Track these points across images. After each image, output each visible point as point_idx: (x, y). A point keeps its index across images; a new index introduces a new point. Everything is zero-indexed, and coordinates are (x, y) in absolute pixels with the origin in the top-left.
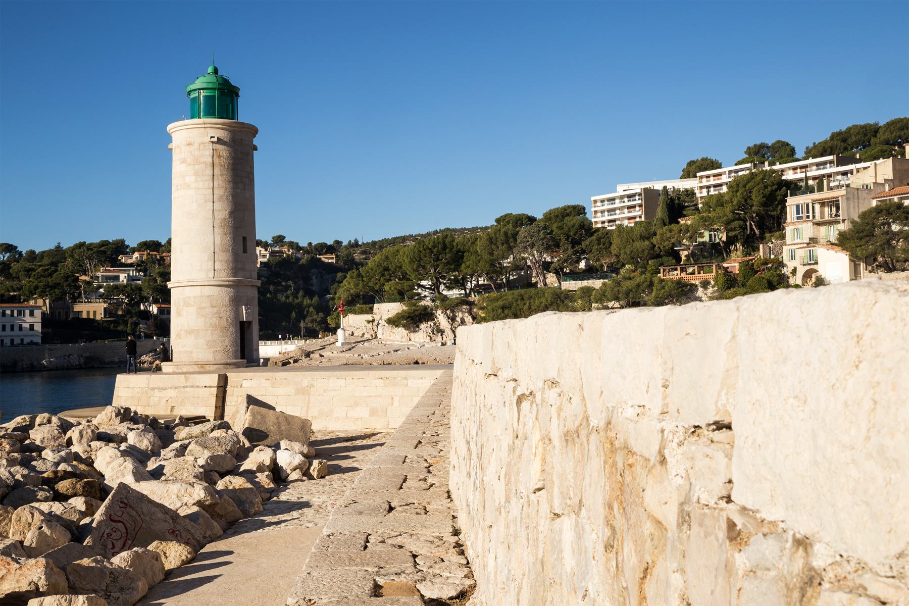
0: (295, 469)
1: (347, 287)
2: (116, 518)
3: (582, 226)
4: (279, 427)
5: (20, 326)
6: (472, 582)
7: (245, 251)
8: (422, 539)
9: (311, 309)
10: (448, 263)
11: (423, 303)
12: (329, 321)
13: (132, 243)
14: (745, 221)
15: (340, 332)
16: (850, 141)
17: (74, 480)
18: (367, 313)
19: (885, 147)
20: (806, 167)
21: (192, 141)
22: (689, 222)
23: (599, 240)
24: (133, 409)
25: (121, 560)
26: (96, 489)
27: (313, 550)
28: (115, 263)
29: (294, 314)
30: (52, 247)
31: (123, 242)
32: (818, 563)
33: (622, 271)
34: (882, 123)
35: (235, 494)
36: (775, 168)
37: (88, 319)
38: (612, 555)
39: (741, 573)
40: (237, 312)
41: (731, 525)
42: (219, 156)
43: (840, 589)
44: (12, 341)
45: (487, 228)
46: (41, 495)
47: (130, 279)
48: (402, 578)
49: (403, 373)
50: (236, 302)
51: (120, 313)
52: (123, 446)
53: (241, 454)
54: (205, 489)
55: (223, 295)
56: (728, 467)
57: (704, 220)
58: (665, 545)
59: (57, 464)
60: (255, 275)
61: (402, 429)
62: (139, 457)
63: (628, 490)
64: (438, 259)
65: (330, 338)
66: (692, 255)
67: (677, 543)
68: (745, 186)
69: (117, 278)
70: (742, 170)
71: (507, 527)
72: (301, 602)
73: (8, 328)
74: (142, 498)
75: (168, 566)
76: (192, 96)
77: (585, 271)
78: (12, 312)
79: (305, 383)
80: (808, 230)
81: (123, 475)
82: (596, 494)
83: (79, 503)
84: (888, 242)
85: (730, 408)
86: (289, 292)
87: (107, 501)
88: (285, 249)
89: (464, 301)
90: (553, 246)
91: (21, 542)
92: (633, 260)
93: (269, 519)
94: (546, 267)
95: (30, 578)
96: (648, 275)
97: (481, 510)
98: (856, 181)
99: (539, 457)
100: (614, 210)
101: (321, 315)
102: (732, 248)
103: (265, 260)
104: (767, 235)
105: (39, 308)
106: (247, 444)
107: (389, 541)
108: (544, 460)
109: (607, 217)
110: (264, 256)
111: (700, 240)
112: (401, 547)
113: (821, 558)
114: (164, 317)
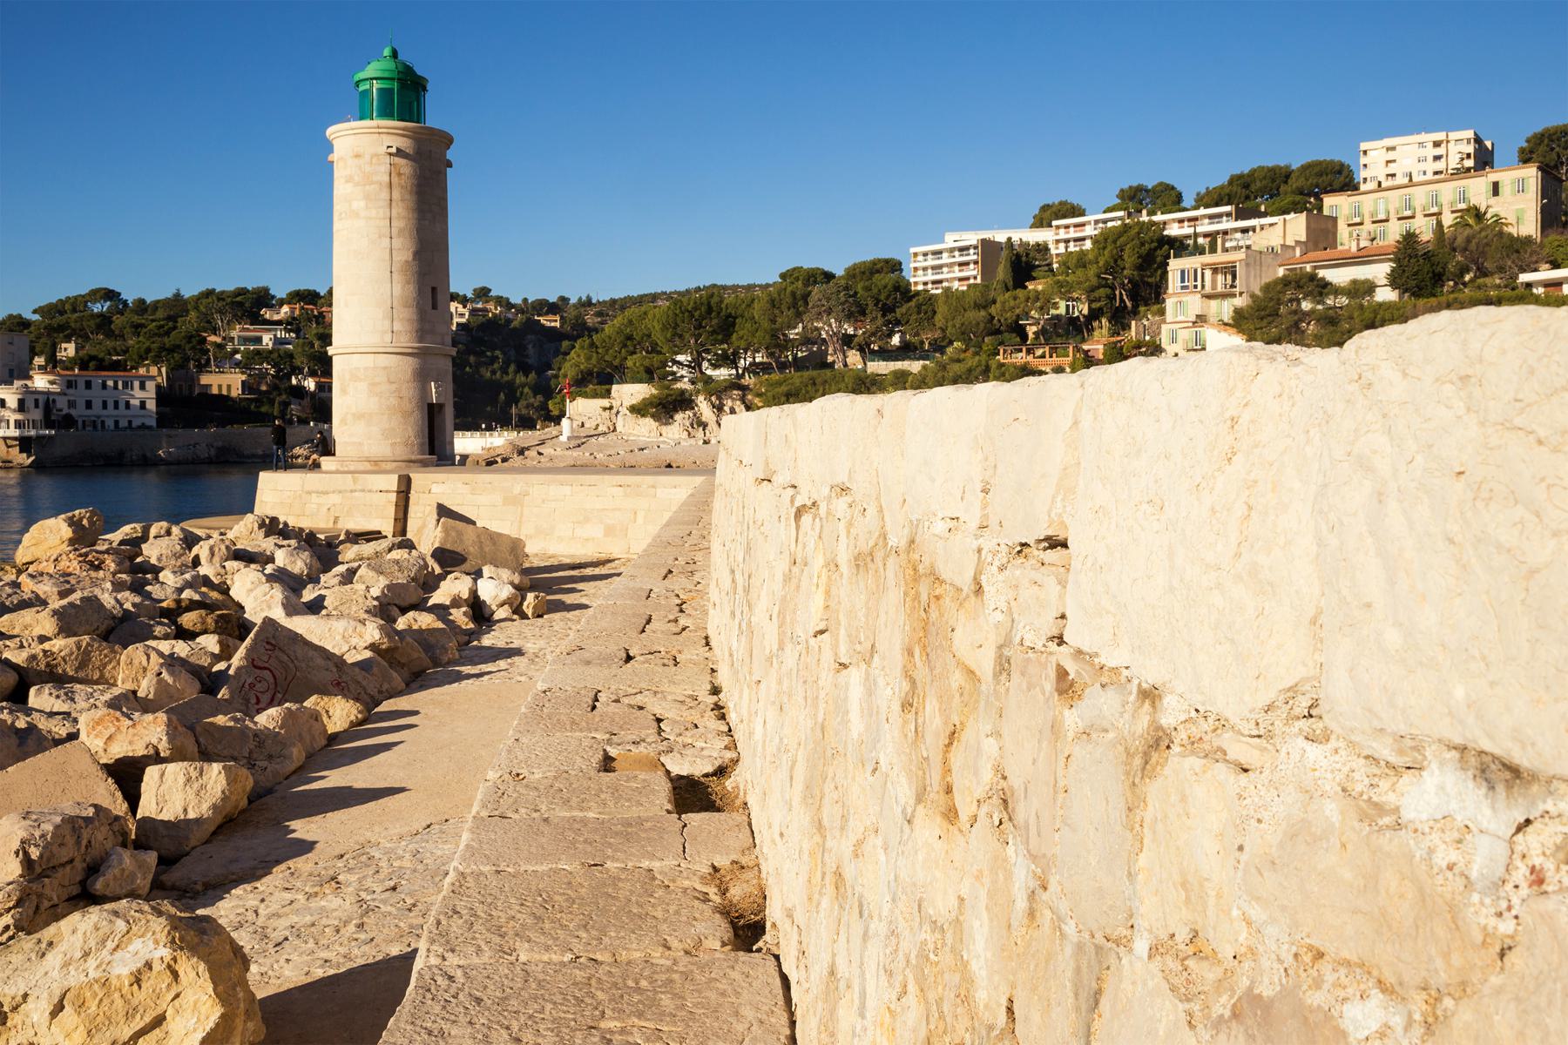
0: (502, 605)
1: (576, 360)
2: (260, 664)
3: (897, 288)
4: (481, 548)
5: (127, 403)
6: (734, 755)
7: (434, 307)
8: (670, 698)
9: (526, 390)
10: (714, 332)
11: (678, 385)
12: (551, 407)
13: (280, 292)
14: (1113, 288)
15: (565, 422)
16: (1253, 188)
17: (203, 612)
18: (603, 397)
19: (1298, 198)
20: (1195, 219)
21: (361, 151)
22: (1040, 288)
23: (919, 306)
24: (282, 519)
25: (268, 719)
26: (233, 625)
27: (523, 710)
28: (256, 319)
29: (502, 396)
30: (169, 294)
31: (266, 290)
32: (1167, 721)
33: (950, 350)
34: (1295, 166)
35: (421, 636)
36: (1155, 218)
37: (220, 396)
38: (911, 716)
39: (1071, 735)
40: (424, 391)
41: (1062, 674)
42: (399, 174)
43: (1193, 753)
44: (117, 422)
45: (768, 285)
46: (159, 630)
47: (277, 341)
48: (642, 748)
49: (649, 479)
50: (422, 376)
51: (264, 388)
52: (269, 569)
53: (429, 583)
54: (381, 628)
55: (407, 365)
56: (1061, 597)
57: (1060, 284)
58: (977, 701)
59: (180, 590)
60: (449, 340)
61: (646, 553)
62: (291, 583)
63: (933, 629)
64: (700, 326)
65: (552, 430)
66: (1043, 332)
67: (992, 699)
68: (1115, 242)
69: (259, 340)
70: (1112, 220)
71: (780, 682)
72: (507, 776)
73: (111, 405)
74: (296, 638)
75: (332, 728)
76: (361, 88)
77: (899, 348)
78: (116, 383)
79: (517, 490)
80: (1194, 305)
81: (270, 607)
82: (893, 635)
83: (210, 642)
84: (1296, 325)
85: (1068, 521)
86: (496, 366)
87: (248, 641)
88: (491, 306)
89: (735, 385)
90: (856, 313)
91: (134, 692)
92: (964, 335)
93: (466, 669)
94: (847, 341)
95: (147, 740)
96: (984, 357)
97: (747, 660)
98: (1260, 241)
99: (822, 589)
100: (940, 267)
101: (540, 398)
102: (1096, 324)
103: (463, 320)
104: (1142, 309)
105: (153, 378)
106: (438, 570)
107: (626, 701)
108: (828, 593)
109: (930, 277)
110: (462, 315)
111: (1053, 312)
112: (641, 708)
113: (1171, 714)
114: (323, 395)
